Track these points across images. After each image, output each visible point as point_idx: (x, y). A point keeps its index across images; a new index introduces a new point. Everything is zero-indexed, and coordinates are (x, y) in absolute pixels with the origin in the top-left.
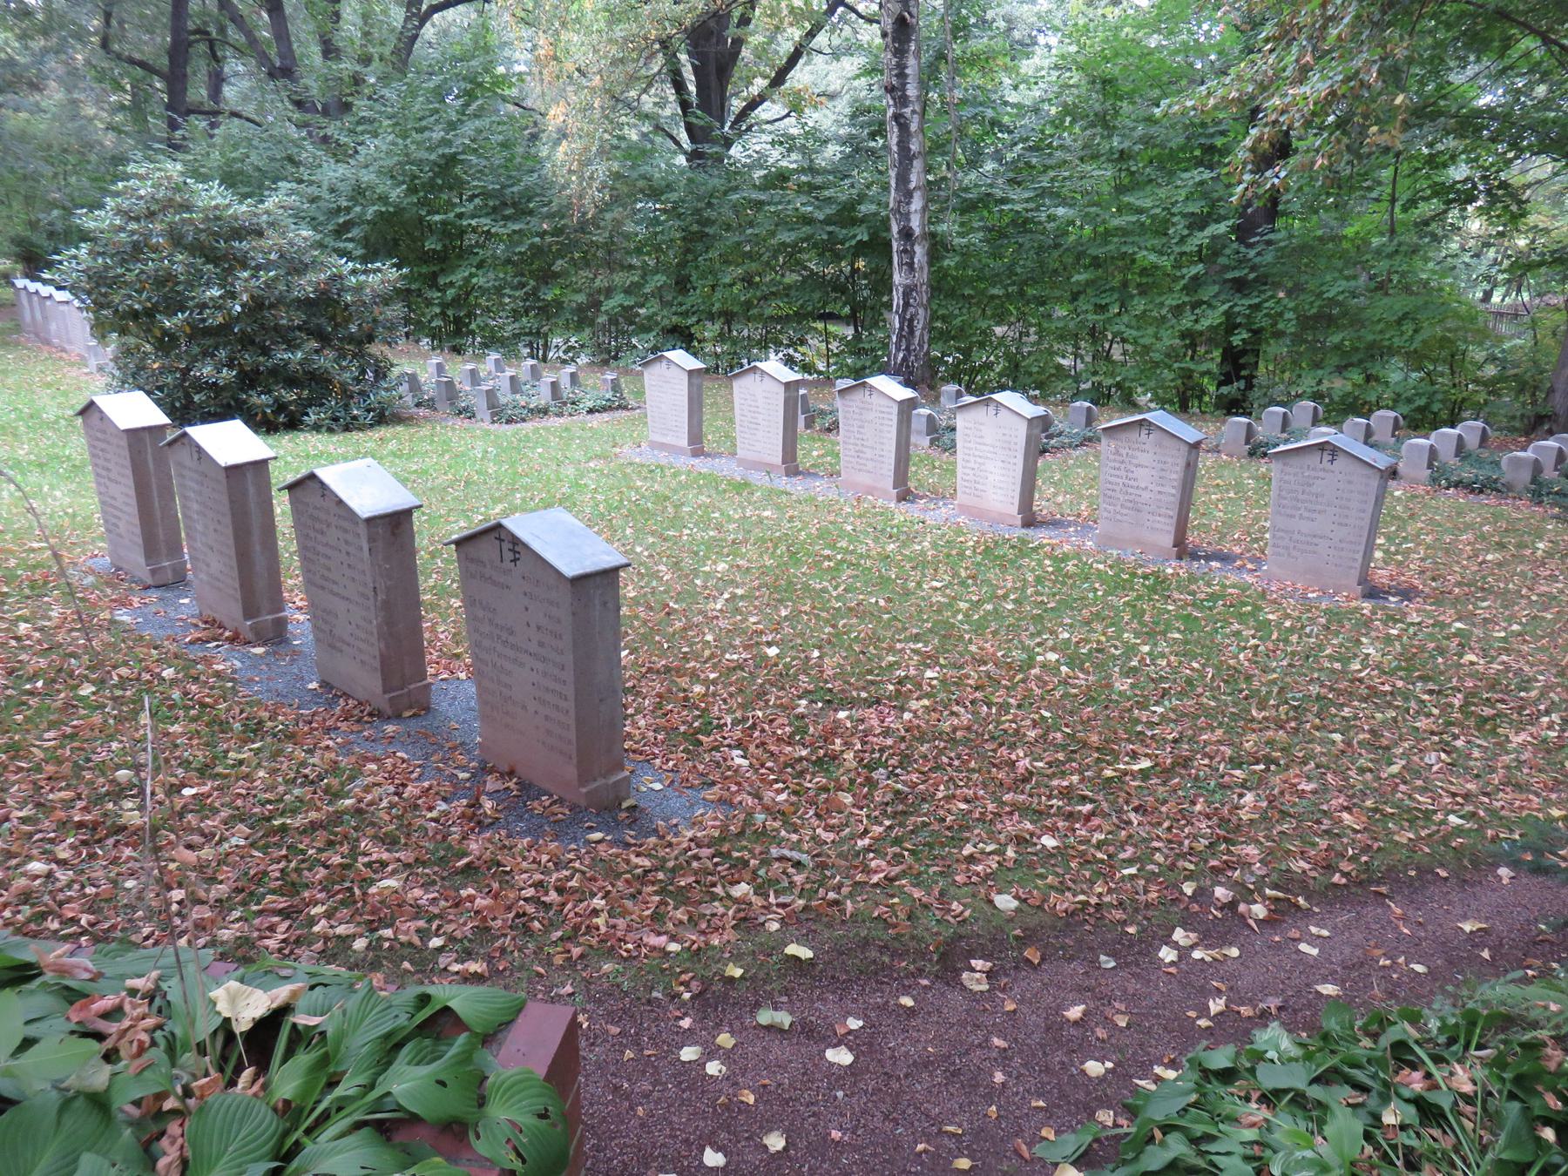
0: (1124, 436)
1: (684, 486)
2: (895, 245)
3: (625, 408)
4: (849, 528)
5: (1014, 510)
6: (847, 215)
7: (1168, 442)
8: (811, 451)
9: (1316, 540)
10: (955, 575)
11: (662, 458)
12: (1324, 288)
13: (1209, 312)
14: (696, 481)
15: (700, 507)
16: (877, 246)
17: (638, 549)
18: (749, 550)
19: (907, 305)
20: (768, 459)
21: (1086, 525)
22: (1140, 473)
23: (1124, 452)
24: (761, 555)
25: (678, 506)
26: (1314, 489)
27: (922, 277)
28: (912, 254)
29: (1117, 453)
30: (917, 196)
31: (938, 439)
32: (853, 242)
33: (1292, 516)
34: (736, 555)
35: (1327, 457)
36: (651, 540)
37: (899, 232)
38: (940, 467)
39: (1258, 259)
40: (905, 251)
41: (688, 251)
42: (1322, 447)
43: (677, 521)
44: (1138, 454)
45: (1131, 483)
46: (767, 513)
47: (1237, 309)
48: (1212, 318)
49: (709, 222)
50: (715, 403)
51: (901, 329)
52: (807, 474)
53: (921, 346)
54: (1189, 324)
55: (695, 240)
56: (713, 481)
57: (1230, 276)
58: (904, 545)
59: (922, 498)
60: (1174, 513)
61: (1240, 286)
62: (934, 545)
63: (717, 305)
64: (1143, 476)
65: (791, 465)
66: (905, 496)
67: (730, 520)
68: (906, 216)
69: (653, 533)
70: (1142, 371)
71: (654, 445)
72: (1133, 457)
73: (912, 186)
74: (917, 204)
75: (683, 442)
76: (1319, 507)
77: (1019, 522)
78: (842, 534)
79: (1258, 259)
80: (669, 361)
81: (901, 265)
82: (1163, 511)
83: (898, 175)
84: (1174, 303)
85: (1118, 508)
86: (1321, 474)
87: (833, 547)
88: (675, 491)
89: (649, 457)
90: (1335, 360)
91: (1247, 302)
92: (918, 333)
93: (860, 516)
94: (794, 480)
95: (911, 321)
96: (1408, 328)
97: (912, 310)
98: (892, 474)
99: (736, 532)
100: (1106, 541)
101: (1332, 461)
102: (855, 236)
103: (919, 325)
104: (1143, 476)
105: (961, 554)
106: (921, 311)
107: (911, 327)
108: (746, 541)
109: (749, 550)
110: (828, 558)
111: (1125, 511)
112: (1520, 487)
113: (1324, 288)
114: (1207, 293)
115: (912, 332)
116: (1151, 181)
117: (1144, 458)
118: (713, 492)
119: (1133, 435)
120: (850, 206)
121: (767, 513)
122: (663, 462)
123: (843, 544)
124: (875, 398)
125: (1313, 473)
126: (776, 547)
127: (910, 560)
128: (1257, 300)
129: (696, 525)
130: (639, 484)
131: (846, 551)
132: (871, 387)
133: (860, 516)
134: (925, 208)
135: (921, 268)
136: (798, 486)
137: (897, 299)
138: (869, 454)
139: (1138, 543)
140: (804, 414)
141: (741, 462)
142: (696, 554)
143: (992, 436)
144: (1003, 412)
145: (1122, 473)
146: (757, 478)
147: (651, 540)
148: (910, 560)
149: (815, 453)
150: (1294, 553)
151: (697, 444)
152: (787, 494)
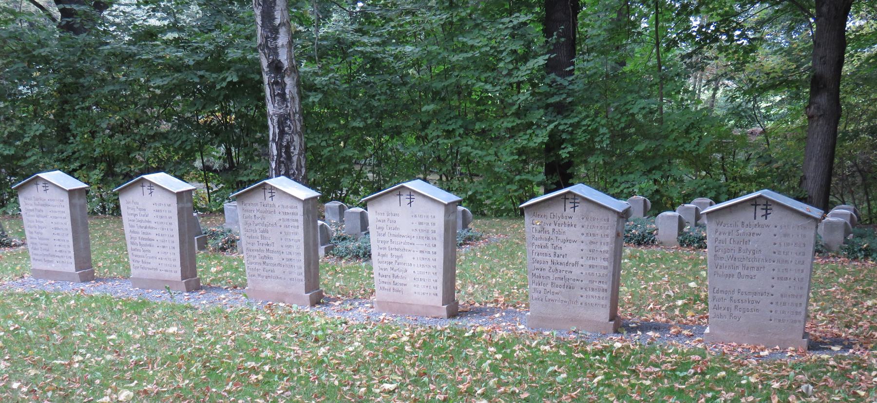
0: (548, 212)
1: (75, 311)
2: (266, 78)
3: (8, 245)
4: (269, 336)
5: (438, 300)
6: (217, 61)
7: (595, 213)
8: (210, 267)
9: (756, 298)
10: (404, 374)
11: (48, 285)
12: (628, 107)
13: (538, 132)
14: (87, 304)
15: (93, 330)
16: (248, 88)
17: (15, 385)
18: (158, 372)
19: (282, 133)
20: (167, 276)
21: (511, 307)
22: (568, 248)
23: (550, 229)
24: (173, 375)
25: (67, 332)
26: (750, 246)
27: (294, 106)
28: (283, 86)
29: (543, 230)
30: (283, 31)
31: (332, 248)
32: (224, 84)
33: (731, 276)
34: (141, 379)
35: (760, 212)
36: (32, 372)
37: (269, 66)
38: (342, 272)
39: (571, 87)
40: (276, 83)
41: (66, 102)
42: (754, 202)
43: (66, 348)
44: (566, 229)
45: (560, 259)
46: (172, 330)
47: (561, 128)
48: (541, 138)
49: (80, 73)
50: (104, 235)
51: (279, 155)
52: (209, 288)
53: (300, 171)
54: (525, 142)
55: (70, 91)
56: (106, 304)
57: (552, 100)
58: (334, 348)
59: (336, 300)
60: (607, 286)
61: (561, 109)
62: (367, 345)
63: (98, 150)
64: (572, 251)
65: (191, 280)
66: (317, 300)
67: (130, 341)
68: (275, 51)
69: (35, 364)
70: (489, 185)
71: (39, 274)
72: (559, 232)
73: (277, 22)
74: (283, 39)
75: (70, 267)
76: (756, 264)
77: (444, 314)
78: (262, 344)
79: (571, 87)
80: (46, 182)
81: (273, 96)
82: (596, 284)
83: (263, 12)
84: (510, 125)
85: (549, 287)
86: (757, 230)
87: (256, 357)
88: (63, 317)
89: (32, 285)
90: (642, 167)
91: (569, 121)
92: (295, 159)
93: (277, 323)
94: (196, 295)
95: (288, 147)
96: (694, 134)
97: (287, 137)
98: (303, 277)
99: (139, 352)
100: (539, 324)
101: (766, 215)
102: (224, 79)
103: (295, 152)
104: (572, 251)
105: (400, 350)
106: (296, 138)
107: (288, 153)
108: (152, 362)
109: (158, 372)
110: (254, 370)
111: (557, 290)
112: (836, 247)
113: (628, 107)
114: (537, 115)
115: (289, 157)
116: (477, 25)
117: (570, 233)
118: (108, 315)
119: (558, 210)
120: (220, 51)
121: (172, 330)
122: (50, 289)
123: (267, 353)
124: (277, 201)
125: (748, 230)
126: (189, 365)
127: (349, 363)
128: (576, 120)
129: (88, 350)
130: (20, 313)
131: (273, 361)
132: (272, 188)
133: (277, 323)
134: (290, 43)
135: (293, 98)
136: (202, 301)
137: (273, 129)
138: (276, 258)
139: (573, 320)
140: (197, 233)
141: (137, 282)
142: (91, 382)
143: (408, 230)
144: (417, 200)
145: (550, 250)
146: (154, 295)
147: (32, 372)
148: (349, 363)
149: (213, 270)
150: (736, 313)
151: (85, 268)
152: (191, 308)
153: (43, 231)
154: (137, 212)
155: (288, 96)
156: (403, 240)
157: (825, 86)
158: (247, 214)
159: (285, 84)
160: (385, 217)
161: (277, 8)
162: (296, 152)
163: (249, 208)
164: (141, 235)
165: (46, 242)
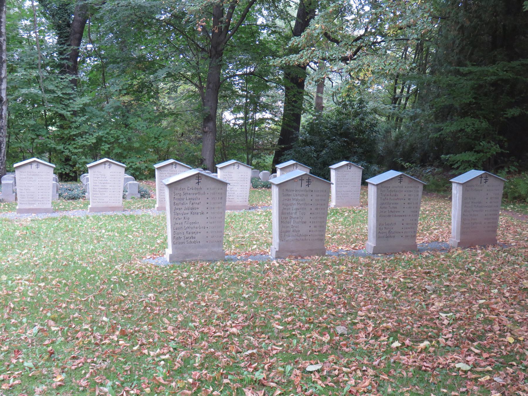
153: (31, 188)
154: (100, 176)
155: (3, 116)
156: (234, 182)
157: (212, 119)
158: (162, 175)
159: (3, 109)
160: (227, 174)
161: (3, 68)
162: (4, 147)
163: (163, 172)
164: (100, 187)
165: (32, 194)
